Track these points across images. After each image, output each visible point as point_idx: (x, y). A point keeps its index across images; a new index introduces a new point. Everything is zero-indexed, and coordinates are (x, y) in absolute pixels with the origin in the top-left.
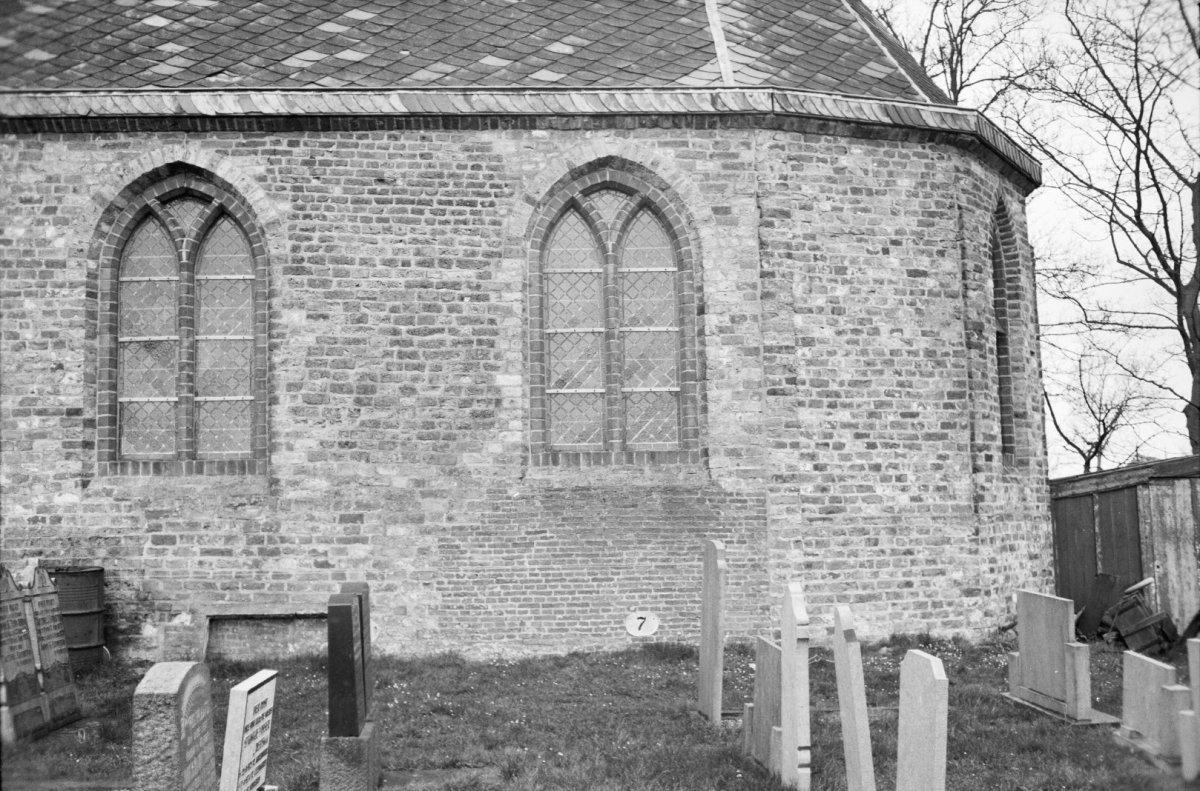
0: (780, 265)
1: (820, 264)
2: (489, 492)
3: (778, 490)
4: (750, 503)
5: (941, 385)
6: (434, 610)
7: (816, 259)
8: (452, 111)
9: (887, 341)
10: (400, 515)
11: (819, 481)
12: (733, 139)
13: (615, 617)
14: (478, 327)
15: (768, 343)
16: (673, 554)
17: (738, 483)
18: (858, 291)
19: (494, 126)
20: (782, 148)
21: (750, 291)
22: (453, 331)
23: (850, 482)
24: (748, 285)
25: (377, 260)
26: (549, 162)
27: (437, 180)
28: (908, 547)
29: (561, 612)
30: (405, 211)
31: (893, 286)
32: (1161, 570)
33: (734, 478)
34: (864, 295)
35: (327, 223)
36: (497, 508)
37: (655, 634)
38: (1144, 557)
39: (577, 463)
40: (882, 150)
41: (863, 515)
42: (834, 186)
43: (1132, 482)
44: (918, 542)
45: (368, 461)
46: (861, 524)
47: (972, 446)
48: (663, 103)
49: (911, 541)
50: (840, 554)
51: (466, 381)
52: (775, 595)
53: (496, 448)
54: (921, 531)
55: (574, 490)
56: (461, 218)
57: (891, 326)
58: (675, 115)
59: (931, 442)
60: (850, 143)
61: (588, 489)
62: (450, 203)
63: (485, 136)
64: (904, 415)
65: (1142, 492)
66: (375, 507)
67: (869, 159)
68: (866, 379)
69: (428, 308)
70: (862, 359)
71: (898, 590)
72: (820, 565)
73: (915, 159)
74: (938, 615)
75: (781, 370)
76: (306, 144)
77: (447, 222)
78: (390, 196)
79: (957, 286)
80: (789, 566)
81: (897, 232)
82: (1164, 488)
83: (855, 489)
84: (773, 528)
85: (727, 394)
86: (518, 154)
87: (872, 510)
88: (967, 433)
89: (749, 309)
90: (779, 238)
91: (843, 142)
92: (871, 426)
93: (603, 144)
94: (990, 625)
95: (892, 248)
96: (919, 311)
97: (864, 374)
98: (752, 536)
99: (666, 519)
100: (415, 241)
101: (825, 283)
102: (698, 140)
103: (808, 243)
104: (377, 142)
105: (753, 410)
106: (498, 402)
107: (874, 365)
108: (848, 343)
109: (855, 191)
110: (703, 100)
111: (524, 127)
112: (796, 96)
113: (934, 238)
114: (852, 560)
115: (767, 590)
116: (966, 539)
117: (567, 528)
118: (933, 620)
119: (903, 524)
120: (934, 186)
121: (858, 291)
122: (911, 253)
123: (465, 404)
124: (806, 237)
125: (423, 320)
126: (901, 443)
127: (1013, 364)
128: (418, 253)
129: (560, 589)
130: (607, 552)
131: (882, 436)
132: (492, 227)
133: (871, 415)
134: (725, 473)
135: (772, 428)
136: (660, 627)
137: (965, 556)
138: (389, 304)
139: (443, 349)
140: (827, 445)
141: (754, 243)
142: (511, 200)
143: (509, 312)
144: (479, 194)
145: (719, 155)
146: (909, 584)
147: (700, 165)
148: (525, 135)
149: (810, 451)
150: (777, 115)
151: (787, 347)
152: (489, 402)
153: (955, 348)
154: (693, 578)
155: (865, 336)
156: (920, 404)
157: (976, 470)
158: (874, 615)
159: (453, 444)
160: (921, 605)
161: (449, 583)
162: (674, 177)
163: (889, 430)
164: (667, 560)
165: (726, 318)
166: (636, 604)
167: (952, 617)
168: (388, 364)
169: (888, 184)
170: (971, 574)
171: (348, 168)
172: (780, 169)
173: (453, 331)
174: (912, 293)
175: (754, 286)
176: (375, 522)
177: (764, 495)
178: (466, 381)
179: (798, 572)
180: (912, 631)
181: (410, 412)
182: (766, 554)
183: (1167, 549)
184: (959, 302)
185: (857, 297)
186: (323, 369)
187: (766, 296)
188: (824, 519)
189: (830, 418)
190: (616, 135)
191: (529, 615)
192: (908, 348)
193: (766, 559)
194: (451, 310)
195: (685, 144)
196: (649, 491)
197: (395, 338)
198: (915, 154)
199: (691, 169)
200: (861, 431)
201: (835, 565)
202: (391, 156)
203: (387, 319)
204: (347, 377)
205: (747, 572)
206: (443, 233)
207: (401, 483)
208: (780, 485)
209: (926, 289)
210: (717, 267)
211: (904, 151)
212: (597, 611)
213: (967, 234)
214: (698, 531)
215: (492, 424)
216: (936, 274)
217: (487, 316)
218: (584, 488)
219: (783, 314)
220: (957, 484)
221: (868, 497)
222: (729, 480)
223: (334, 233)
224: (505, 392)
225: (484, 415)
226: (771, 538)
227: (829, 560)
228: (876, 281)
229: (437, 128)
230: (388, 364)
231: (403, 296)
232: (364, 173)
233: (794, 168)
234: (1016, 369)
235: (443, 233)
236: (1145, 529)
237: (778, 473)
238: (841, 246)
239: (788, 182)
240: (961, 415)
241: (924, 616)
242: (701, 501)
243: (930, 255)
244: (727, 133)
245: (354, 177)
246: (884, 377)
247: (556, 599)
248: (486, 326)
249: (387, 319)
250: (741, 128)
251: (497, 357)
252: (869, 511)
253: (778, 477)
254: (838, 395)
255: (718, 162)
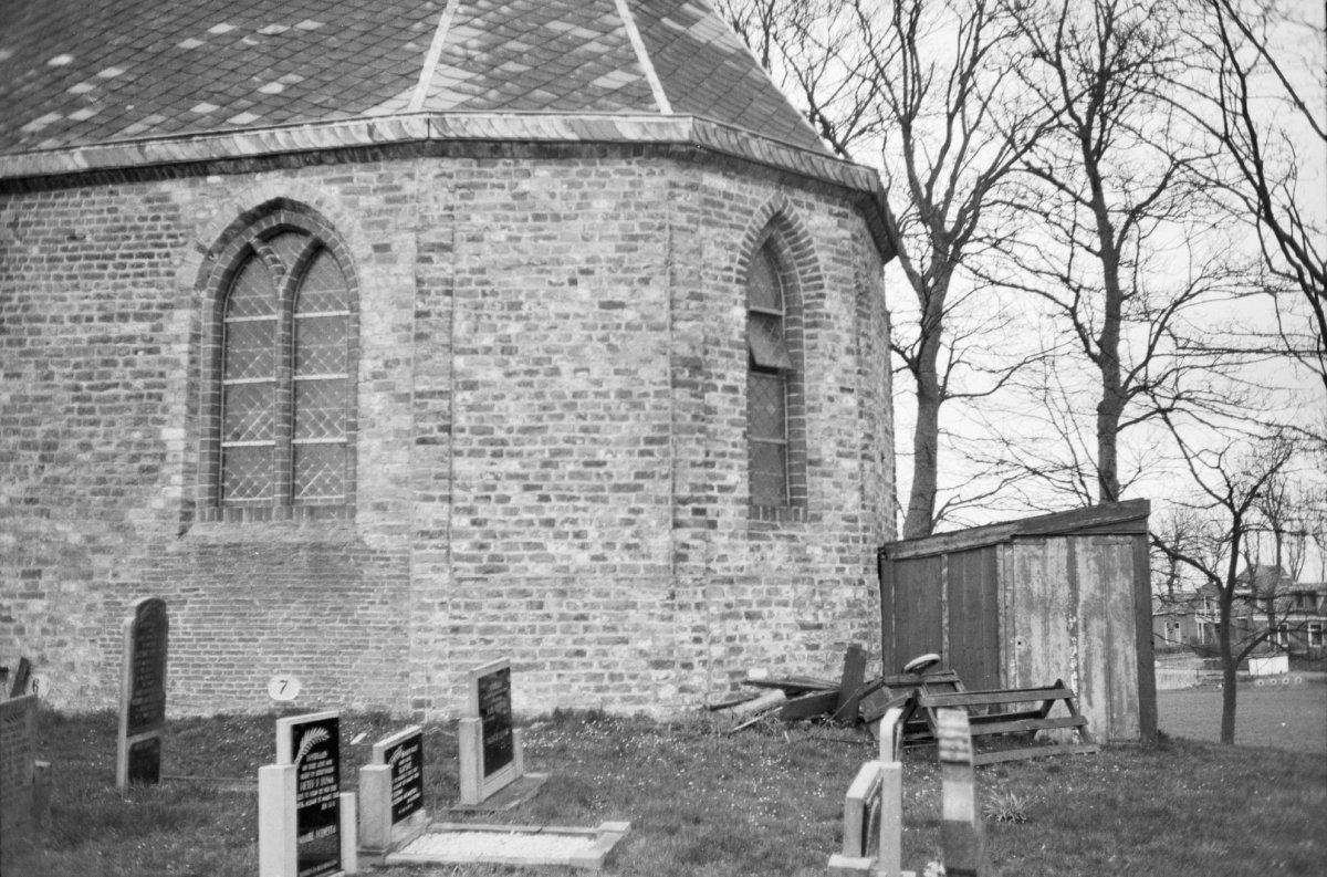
0: (437, 303)
1: (490, 300)
2: (150, 548)
3: (423, 547)
4: (394, 562)
5: (636, 430)
6: (97, 667)
7: (484, 294)
8: (127, 163)
9: (569, 382)
10: (72, 570)
11: (477, 537)
12: (395, 170)
13: (258, 679)
14: (149, 380)
15: (420, 388)
16: (316, 614)
17: (383, 539)
18: (536, 328)
19: (172, 176)
20: (451, 176)
21: (404, 332)
22: (127, 386)
23: (515, 539)
24: (404, 327)
25: (66, 316)
26: (221, 208)
27: (120, 234)
28: (582, 611)
29: (208, 673)
30: (90, 267)
31: (580, 320)
32: (1023, 647)
33: (379, 535)
34: (542, 331)
35: (25, 283)
36: (156, 565)
37: (297, 698)
38: (1002, 631)
39: (240, 518)
40: (575, 169)
41: (528, 575)
42: (510, 213)
43: (990, 540)
44: (594, 606)
45: (48, 516)
46: (523, 586)
47: (674, 498)
48: (321, 139)
49: (585, 605)
50: (495, 618)
51: (137, 435)
52: (416, 660)
53: (158, 503)
54: (598, 594)
55: (226, 547)
56: (140, 270)
57: (574, 366)
58: (335, 151)
59: (621, 494)
60: (535, 165)
61: (239, 545)
62: (130, 256)
63: (165, 186)
64: (587, 464)
65: (1000, 552)
66: (52, 563)
67: (557, 181)
68: (540, 424)
69: (106, 363)
70: (536, 402)
71: (566, 659)
72: (469, 629)
73: (618, 176)
74: (617, 689)
75: (433, 417)
76: (12, 207)
77: (127, 276)
78: (79, 253)
79: (663, 317)
80: (432, 630)
81: (588, 260)
82: (1032, 548)
83: (521, 546)
84: (418, 588)
85: (377, 443)
86: (193, 202)
87: (540, 569)
88: (668, 484)
89: (404, 352)
90: (438, 274)
91: (526, 164)
92: (545, 477)
93: (271, 186)
94: (688, 705)
95: (580, 278)
96: (612, 348)
97: (539, 419)
98: (394, 597)
99: (312, 577)
100: (99, 296)
101: (494, 320)
102: (363, 174)
103: (476, 278)
104: (71, 200)
105: (400, 461)
106: (163, 457)
107: (553, 408)
108: (519, 385)
109: (537, 217)
110: (359, 132)
111: (199, 174)
112: (456, 120)
113: (636, 265)
114: (509, 625)
115: (407, 655)
116: (657, 604)
117: (218, 585)
118: (609, 694)
119: (577, 585)
120: (639, 206)
121: (536, 328)
122: (605, 283)
123: (135, 458)
124: (473, 271)
125: (102, 375)
126: (582, 495)
127: (808, 403)
128: (100, 308)
129: (208, 648)
130: (253, 611)
131: (557, 488)
132: (166, 279)
133: (546, 464)
134: (369, 528)
135: (418, 480)
136: (302, 692)
137: (655, 623)
138: (73, 360)
139: (117, 404)
140: (488, 498)
141: (410, 281)
142: (185, 249)
143: (176, 364)
144: (156, 245)
145: (383, 189)
146: (580, 653)
147: (364, 201)
148: (201, 182)
149: (467, 504)
150: (437, 141)
151: (441, 393)
152: (155, 456)
153: (657, 388)
154: (335, 640)
155: (540, 377)
156: (609, 452)
157: (677, 525)
158: (534, 685)
159: (121, 500)
160: (594, 677)
161: (111, 640)
162: (337, 216)
163: (567, 481)
164: (309, 621)
165: (380, 363)
166: (279, 666)
167: (635, 692)
168: (69, 421)
169: (579, 207)
170: (662, 643)
171: (46, 227)
172: (446, 199)
173: (127, 386)
174: (604, 327)
175: (408, 328)
176: (50, 578)
177: (408, 552)
178: (137, 435)
179: (442, 636)
180: (581, 706)
181: (86, 468)
182: (409, 616)
183: (1032, 622)
184: (665, 336)
185: (533, 334)
186: (14, 427)
187: (420, 337)
188: (477, 579)
189: (494, 468)
190: (286, 175)
191: (180, 674)
192: (596, 389)
193: (407, 622)
194: (128, 363)
195: (350, 179)
196: (298, 547)
197: (76, 394)
198: (617, 171)
199: (353, 205)
200: (531, 481)
201: (487, 630)
202: (83, 213)
203: (70, 376)
204: (34, 434)
205: (387, 636)
206: (123, 286)
207: (75, 539)
208: (425, 542)
209: (623, 323)
210: (374, 309)
211: (603, 169)
212: (241, 673)
213: (677, 257)
214: (341, 590)
215: (155, 479)
216: (637, 305)
217: (159, 368)
218: (235, 545)
219: (438, 357)
220: (652, 542)
221: (537, 555)
222: (374, 536)
223: (31, 293)
224: (170, 446)
225: (149, 469)
226: (414, 599)
227: (481, 624)
228: (558, 315)
229: (122, 182)
230: (69, 421)
231: (85, 351)
232: (58, 231)
233: (463, 197)
234: (812, 409)
235: (123, 286)
236: (1003, 596)
237: (425, 529)
238: (517, 279)
239: (455, 213)
240: (660, 463)
241: (599, 689)
242: (345, 558)
243: (630, 283)
244: (393, 165)
245: (50, 236)
246: (565, 422)
247: (204, 660)
248: (156, 380)
249: (70, 376)
250: (405, 157)
251: (165, 410)
252: (537, 570)
253: (424, 533)
254: (504, 442)
255: (381, 196)
